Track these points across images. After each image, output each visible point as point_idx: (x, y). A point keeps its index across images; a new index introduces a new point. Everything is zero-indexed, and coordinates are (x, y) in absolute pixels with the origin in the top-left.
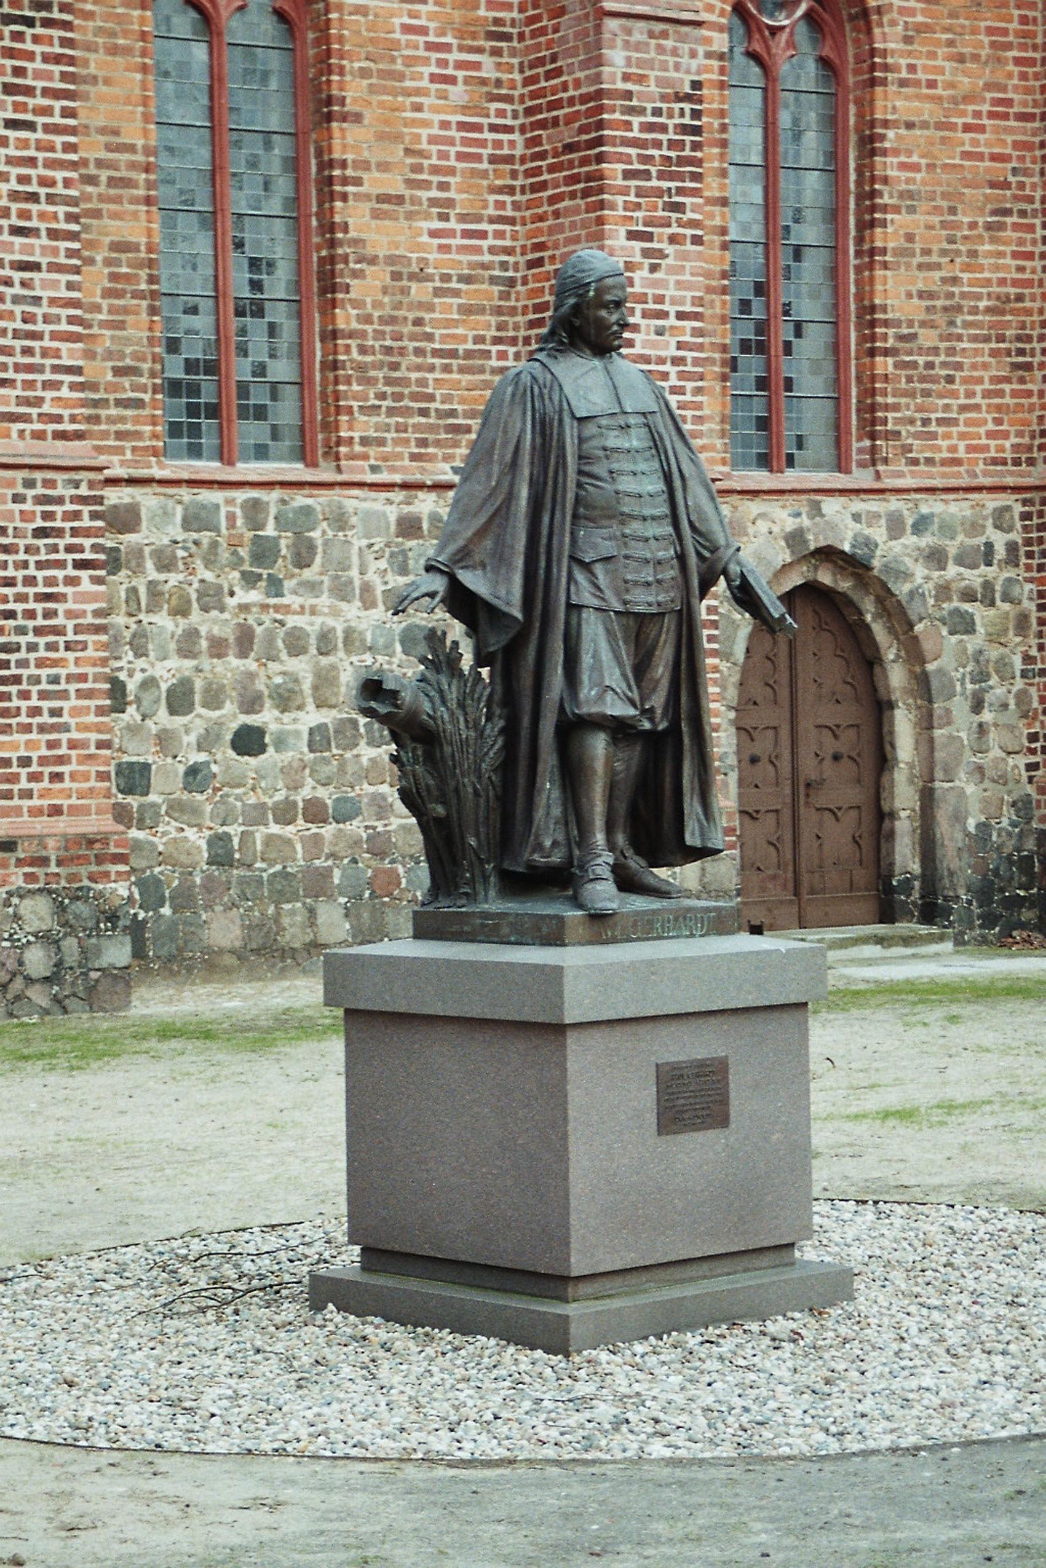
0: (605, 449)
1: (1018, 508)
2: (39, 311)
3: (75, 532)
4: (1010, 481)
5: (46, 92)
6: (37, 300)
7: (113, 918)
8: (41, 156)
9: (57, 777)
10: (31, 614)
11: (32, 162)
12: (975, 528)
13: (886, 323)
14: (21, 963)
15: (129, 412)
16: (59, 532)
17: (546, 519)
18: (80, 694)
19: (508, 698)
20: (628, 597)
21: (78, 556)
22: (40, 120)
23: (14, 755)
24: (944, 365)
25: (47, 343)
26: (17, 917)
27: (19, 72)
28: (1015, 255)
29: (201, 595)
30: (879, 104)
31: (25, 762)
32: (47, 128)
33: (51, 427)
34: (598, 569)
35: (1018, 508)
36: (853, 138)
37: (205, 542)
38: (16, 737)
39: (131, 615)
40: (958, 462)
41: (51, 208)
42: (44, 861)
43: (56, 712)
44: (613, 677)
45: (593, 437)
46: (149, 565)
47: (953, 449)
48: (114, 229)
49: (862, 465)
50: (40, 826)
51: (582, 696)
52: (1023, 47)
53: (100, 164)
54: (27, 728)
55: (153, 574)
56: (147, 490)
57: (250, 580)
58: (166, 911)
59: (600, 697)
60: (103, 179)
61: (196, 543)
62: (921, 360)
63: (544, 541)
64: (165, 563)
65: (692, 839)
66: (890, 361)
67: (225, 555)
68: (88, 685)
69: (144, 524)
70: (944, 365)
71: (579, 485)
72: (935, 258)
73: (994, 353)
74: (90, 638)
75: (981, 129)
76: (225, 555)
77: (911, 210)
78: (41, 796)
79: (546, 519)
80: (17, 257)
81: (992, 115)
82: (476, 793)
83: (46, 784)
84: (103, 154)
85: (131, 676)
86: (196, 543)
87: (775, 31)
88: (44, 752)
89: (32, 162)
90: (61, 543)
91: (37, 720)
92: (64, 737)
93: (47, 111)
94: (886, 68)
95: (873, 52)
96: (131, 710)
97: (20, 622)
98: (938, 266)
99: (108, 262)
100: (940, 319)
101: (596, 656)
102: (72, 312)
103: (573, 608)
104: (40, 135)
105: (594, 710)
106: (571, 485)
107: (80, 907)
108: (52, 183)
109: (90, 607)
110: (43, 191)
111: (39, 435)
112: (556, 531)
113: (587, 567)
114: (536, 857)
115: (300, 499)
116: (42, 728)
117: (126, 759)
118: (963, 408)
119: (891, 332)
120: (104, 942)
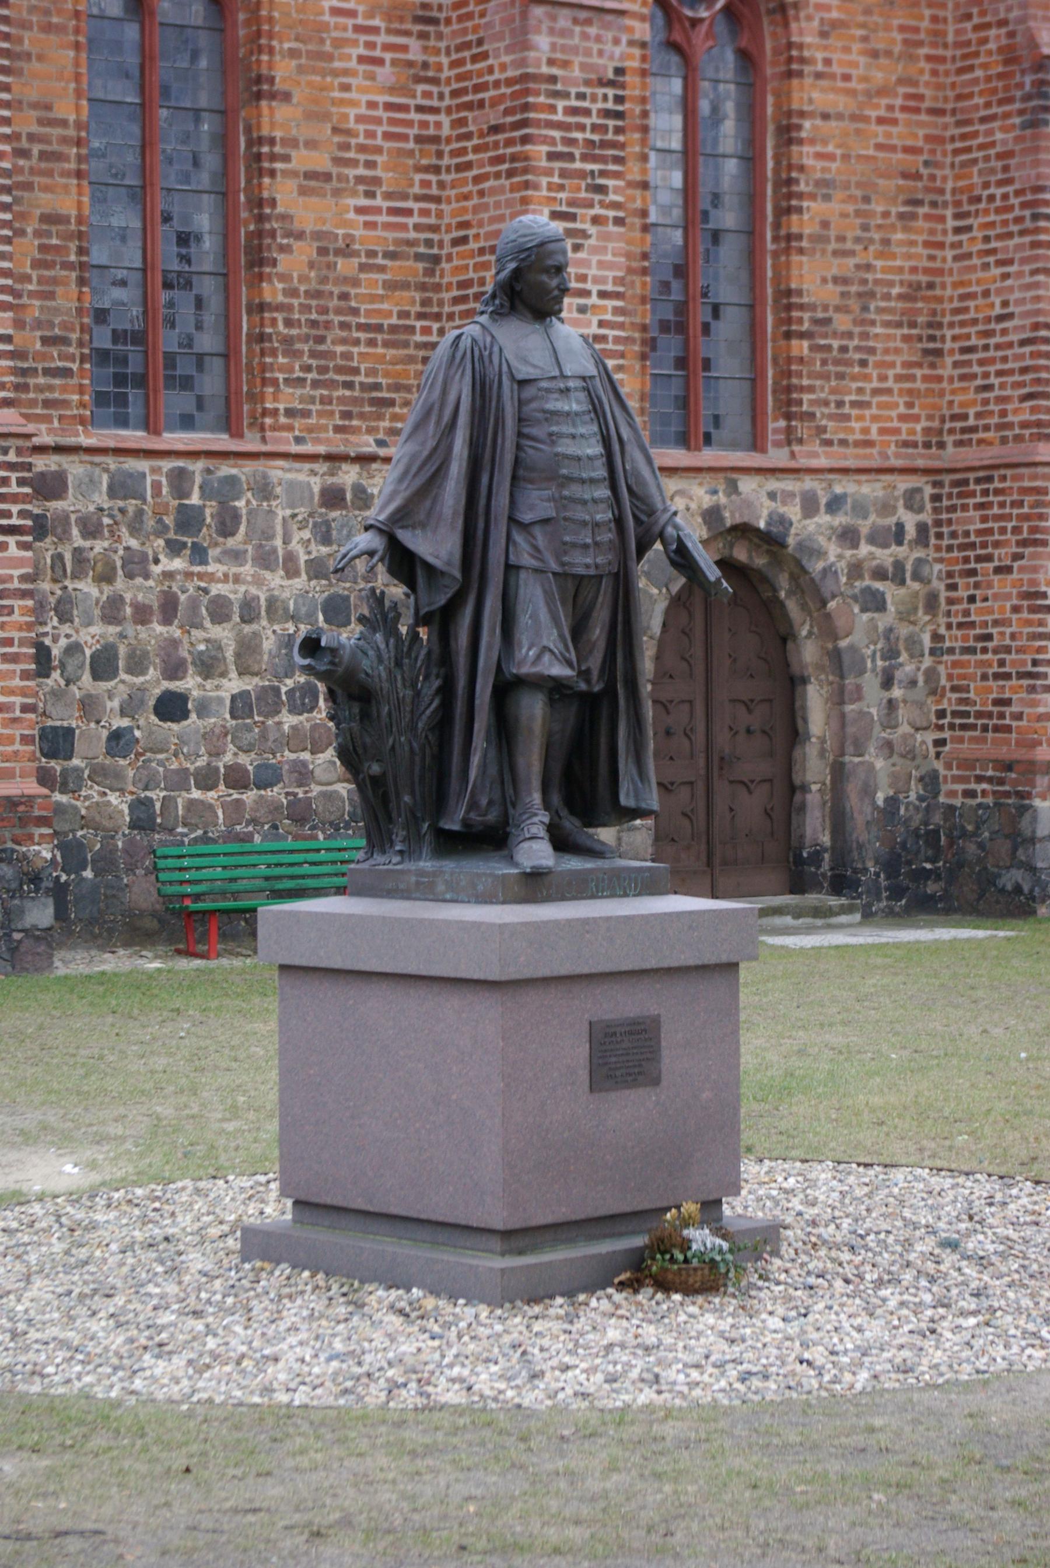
1: (928, 490)
4: (920, 463)
7: (35, 879)
12: (886, 508)
13: (802, 307)
15: (57, 382)
24: (858, 349)
30: (795, 95)
35: (928, 490)
36: (771, 128)
37: (131, 510)
40: (869, 444)
44: (551, 638)
46: (75, 532)
47: (866, 431)
48: (44, 201)
49: (777, 444)
52: (934, 45)
53: (31, 137)
55: (79, 542)
56: (75, 458)
57: (174, 548)
58: (88, 874)
59: (539, 657)
60: (35, 152)
61: (122, 511)
62: (836, 344)
64: (91, 530)
66: (805, 344)
67: (150, 523)
70: (858, 349)
71: (519, 447)
72: (849, 245)
73: (906, 338)
76: (150, 523)
77: (827, 198)
84: (35, 128)
85: (55, 640)
86: (122, 511)
94: (802, 60)
96: (56, 675)
99: (38, 234)
101: (534, 617)
105: (534, 670)
109: (16, 573)
117: (50, 723)
119: (806, 316)
120: (28, 904)
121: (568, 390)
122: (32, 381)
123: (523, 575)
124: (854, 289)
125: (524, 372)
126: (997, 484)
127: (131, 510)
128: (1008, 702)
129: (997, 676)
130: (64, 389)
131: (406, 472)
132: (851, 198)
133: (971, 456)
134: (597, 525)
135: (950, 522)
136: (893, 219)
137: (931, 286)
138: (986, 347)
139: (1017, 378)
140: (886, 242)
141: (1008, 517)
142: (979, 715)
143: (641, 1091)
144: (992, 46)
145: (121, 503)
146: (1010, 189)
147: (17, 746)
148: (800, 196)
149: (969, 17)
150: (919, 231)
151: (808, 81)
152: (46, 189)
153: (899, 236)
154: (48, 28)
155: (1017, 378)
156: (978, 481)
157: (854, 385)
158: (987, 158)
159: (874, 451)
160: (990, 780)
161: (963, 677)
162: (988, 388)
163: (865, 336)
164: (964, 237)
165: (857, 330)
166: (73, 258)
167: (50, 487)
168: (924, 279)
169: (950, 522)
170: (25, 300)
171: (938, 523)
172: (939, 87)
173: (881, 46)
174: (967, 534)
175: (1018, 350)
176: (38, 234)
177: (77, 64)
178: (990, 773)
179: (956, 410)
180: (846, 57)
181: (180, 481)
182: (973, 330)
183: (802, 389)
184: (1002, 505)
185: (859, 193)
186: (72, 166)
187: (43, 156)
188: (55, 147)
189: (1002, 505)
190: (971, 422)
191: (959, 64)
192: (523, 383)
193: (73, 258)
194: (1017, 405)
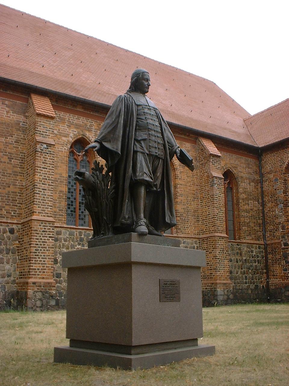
0: (144, 113)
1: (198, 241)
2: (46, 197)
3: (49, 232)
4: (197, 237)
5: (49, 164)
6: (45, 195)
7: (52, 296)
8: (48, 173)
9: (44, 272)
10: (41, 245)
11: (47, 174)
12: (192, 244)
13: (178, 212)
14: (36, 304)
15: (61, 216)
16: (46, 232)
17: (128, 129)
18: (49, 258)
19: (116, 179)
20: (150, 150)
21: (49, 235)
23: (36, 268)
24: (187, 219)
25: (47, 201)
26: (35, 296)
27: (45, 160)
28: (196, 204)
29: (71, 246)
30: (177, 182)
31: (38, 269)
32: (49, 169)
33: (46, 215)
34: (142, 142)
35: (198, 241)
36: (173, 186)
37: (72, 238)
38: (37, 265)
39: (59, 248)
40: (189, 234)
41: (49, 181)
42: (41, 286)
43: (44, 261)
44: (146, 170)
45: (141, 110)
46: (63, 240)
47: (189, 232)
48: (60, 189)
49: (175, 233)
50: (41, 280)
51: (137, 174)
52: (196, 176)
53: (58, 179)
54: (39, 264)
55: (63, 242)
56: (63, 228)
57: (79, 244)
58: (63, 298)
59: (143, 175)
60: (59, 181)
61: (71, 238)
62: (184, 218)
63: (127, 134)
64: (65, 241)
65: (167, 220)
66: (179, 218)
67: (75, 240)
68: (50, 257)
69: (62, 234)
70: (187, 219)
71: (137, 121)
72: (185, 204)
73: (194, 218)
74: (51, 249)
75: (191, 186)
76: (75, 240)
77: (182, 197)
78: (41, 275)
79: (128, 129)
80: (43, 188)
81: (192, 185)
82: (106, 203)
83: (42, 273)
84: (59, 177)
85: (59, 258)
86: (71, 238)
87: (79, 155)
88: (42, 268)
90: (47, 233)
91: (41, 262)
92: (45, 265)
94: (177, 176)
95: (175, 174)
96: (59, 264)
97: (39, 246)
98: (186, 205)
99: (59, 193)
100: (186, 212)
101: (141, 164)
102: (51, 197)
103: (135, 152)
104: (48, 170)
105: (141, 178)
106: (135, 120)
107: (47, 295)
108: (49, 177)
109: (51, 244)
110: (48, 178)
111: (45, 216)
112: (130, 138)
113: (139, 141)
114: (123, 220)
115: (88, 232)
116: (42, 264)
117: (57, 272)
118: (190, 226)
119: (179, 214)
120: (50, 301)
121: (150, 109)
122: (57, 216)
123: (138, 153)
124: (186, 210)
125: (138, 103)
126: (209, 240)
127: (72, 238)
128: (212, 274)
129: (210, 270)
130: (62, 218)
131: (106, 127)
132: (185, 197)
133: (205, 236)
134: (159, 143)
135: (202, 246)
136: (191, 200)
137: (197, 211)
138: (206, 219)
139: (211, 223)
140: (191, 204)
141: (211, 245)
142: (207, 276)
143: (174, 303)
144: (205, 175)
145: (70, 236)
146: (209, 196)
147: (50, 273)
148: (178, 196)
149: (202, 172)
150: (195, 203)
151: (178, 179)
152: (61, 187)
153: (192, 203)
154: (62, 163)
155: (211, 223)
156: (206, 239)
157: (186, 225)
158: (205, 192)
159: (190, 235)
160: (209, 286)
161: (204, 270)
162: (207, 225)
163: (188, 217)
164: (202, 203)
165: (187, 216)
166: (64, 197)
167: (59, 233)
168: (196, 210)
169: (202, 246)
170: (56, 203)
171: (200, 246)
172: (197, 182)
173: (189, 175)
174: (204, 248)
175: (211, 219)
176: (59, 193)
177: (66, 168)
178: (209, 285)
179: (202, 229)
180: (184, 177)
181: (80, 234)
182: (204, 217)
183: (179, 225)
184: (210, 243)
185: (186, 196)
186: (65, 183)
187: (60, 182)
188: (62, 180)
189: (210, 243)
190: (204, 230)
191: (200, 179)
192: (138, 105)
193: (64, 197)
194: (212, 227)
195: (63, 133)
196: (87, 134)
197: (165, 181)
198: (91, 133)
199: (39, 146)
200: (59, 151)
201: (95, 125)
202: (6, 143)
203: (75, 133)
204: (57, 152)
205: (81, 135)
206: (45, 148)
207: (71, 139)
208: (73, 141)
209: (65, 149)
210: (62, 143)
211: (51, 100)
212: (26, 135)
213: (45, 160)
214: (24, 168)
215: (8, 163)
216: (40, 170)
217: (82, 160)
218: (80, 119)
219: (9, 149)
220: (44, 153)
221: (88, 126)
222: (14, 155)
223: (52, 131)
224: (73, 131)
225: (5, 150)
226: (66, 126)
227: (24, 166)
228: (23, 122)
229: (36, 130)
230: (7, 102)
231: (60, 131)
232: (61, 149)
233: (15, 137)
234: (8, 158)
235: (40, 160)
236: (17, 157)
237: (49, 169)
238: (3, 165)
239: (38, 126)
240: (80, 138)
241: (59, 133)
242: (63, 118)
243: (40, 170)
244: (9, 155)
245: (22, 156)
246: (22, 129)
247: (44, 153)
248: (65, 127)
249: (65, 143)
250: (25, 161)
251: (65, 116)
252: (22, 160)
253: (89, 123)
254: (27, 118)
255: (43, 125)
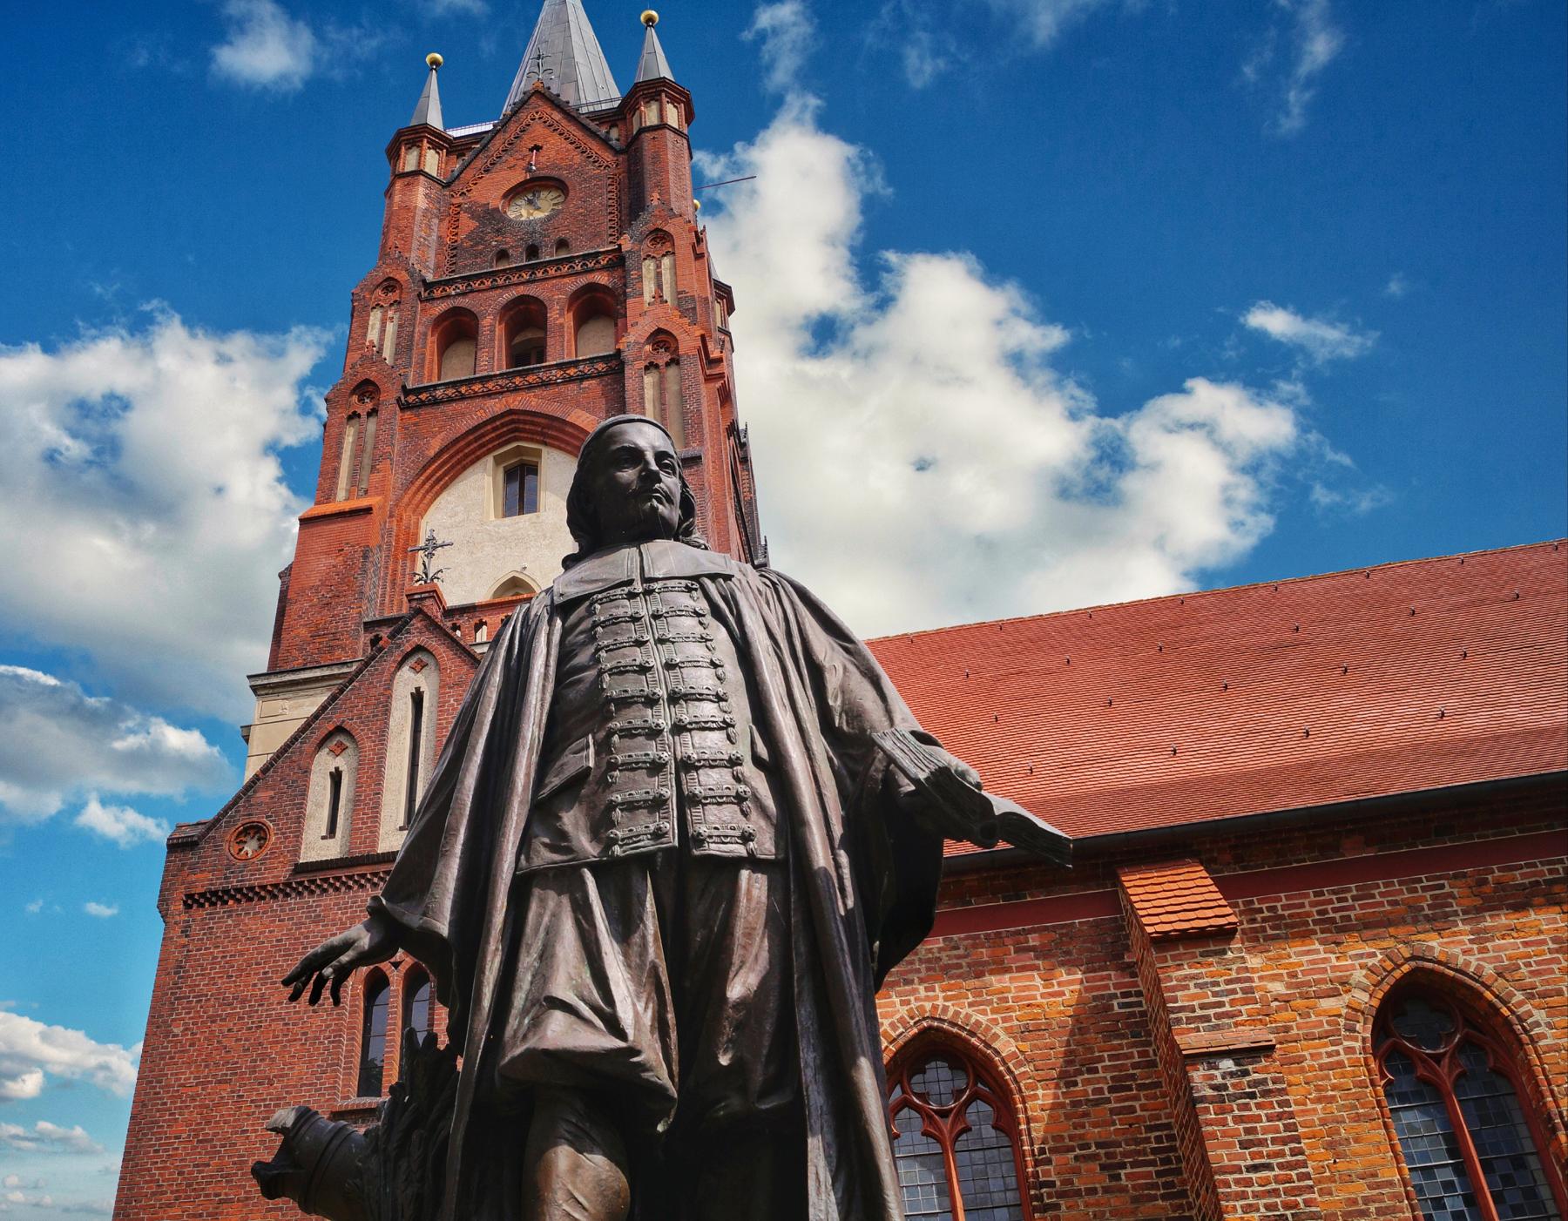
5: (1274, 1141)
11: (1275, 1192)
22: (1274, 1161)
32: (1281, 1166)
53: (1367, 1201)
60: (1372, 1209)
84: (1368, 1193)
87: (1438, 1058)
89: (1275, 1192)
93: (1281, 1154)
104: (1277, 1172)
154: (1357, 1118)
195: (1317, 982)
196: (1432, 948)
197: (486, 1002)
198: (1455, 934)
199: (1201, 1072)
200: (1321, 1067)
201: (1455, 891)
202: (1075, 1104)
203: (1370, 962)
204: (1317, 1078)
205: (1407, 960)
206: (1232, 1074)
207: (1365, 997)
208: (1375, 1003)
209: (1349, 1050)
210: (1327, 1027)
211: (1209, 865)
212: (1149, 1044)
213: (1248, 1131)
214: (1183, 1194)
215: (1106, 1190)
216: (1237, 1182)
217: (1462, 1075)
218: (1376, 892)
219: (1095, 1125)
220: (1236, 1097)
221: (1427, 912)
222: (1124, 1147)
223: (1244, 991)
224: (1361, 956)
225: (1081, 1137)
226: (1317, 946)
227: (1184, 1182)
228: (1124, 995)
229: (1174, 1010)
230: (1033, 940)
231: (1301, 978)
232: (1329, 1055)
233: (1105, 1069)
234: (1103, 1167)
235: (1224, 1134)
236: (1139, 1153)
237: (1281, 1166)
238: (1087, 1205)
239: (1173, 989)
240: (1405, 975)
241: (1299, 985)
242: (1291, 916)
243: (1237, 1182)
244: (1102, 1151)
245: (1159, 1139)
246: (1128, 1026)
247: (1236, 1097)
248: (1317, 952)
249: (1342, 1021)
250: (1179, 1160)
251: (1302, 905)
252: (1163, 1161)
253: (1427, 895)
254: (1134, 975)
255: (1188, 984)
